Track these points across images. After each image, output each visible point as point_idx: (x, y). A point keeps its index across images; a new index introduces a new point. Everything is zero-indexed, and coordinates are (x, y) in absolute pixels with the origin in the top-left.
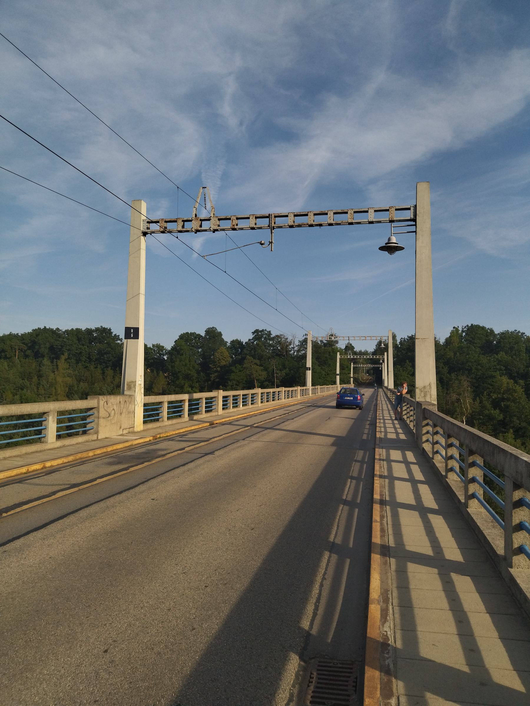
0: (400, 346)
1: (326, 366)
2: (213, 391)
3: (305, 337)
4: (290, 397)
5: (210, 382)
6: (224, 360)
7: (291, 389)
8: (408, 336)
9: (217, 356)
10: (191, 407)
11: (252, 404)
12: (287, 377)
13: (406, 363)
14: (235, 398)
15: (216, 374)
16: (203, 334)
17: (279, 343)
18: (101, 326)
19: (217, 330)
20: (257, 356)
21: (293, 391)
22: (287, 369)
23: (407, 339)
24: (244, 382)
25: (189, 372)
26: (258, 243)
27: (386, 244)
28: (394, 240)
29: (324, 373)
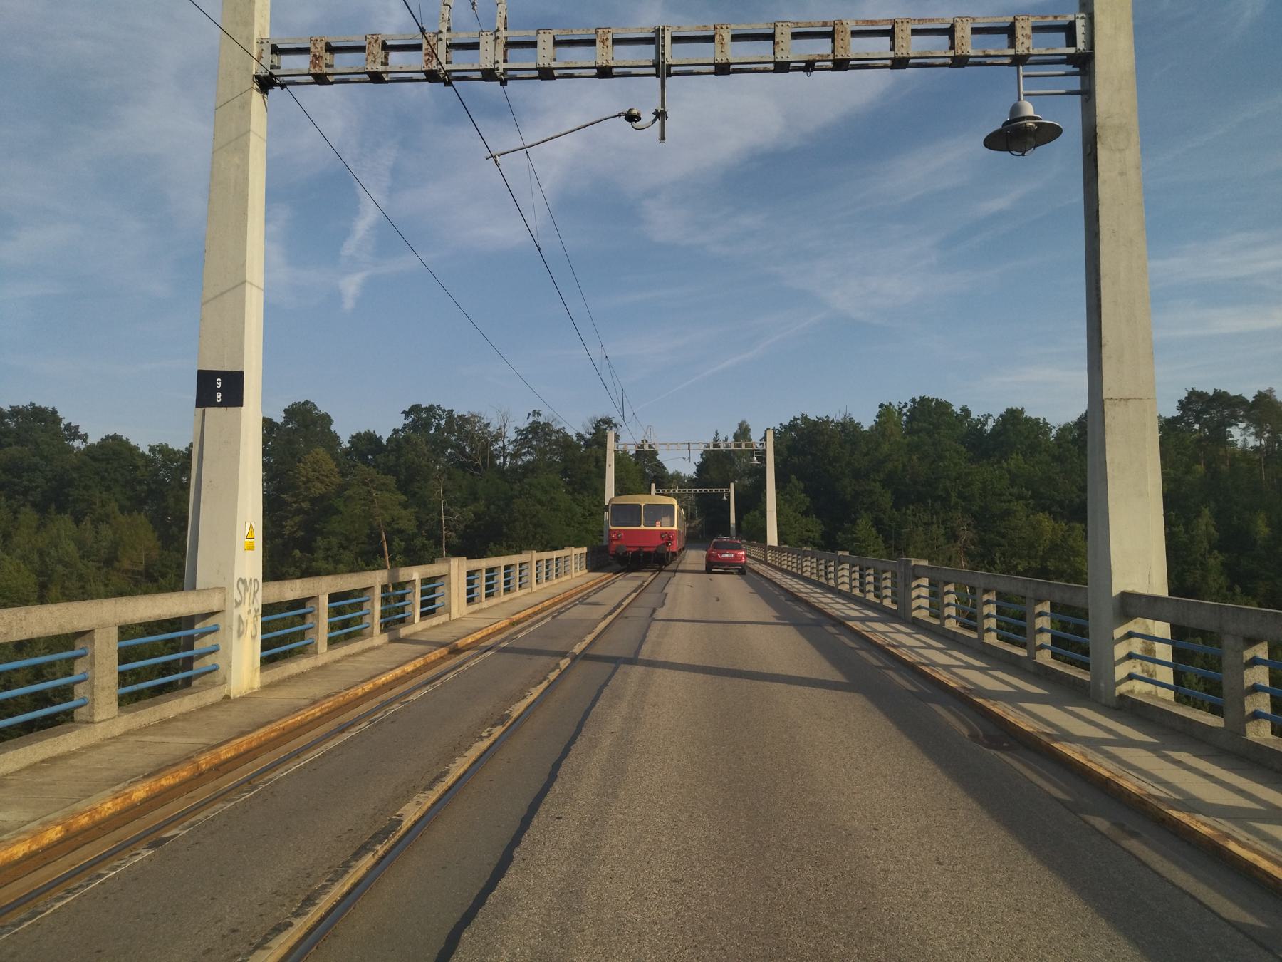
0: (1051, 440)
1: (586, 493)
2: (523, 552)
3: (532, 419)
4: (561, 573)
5: (278, 541)
6: (322, 482)
7: (554, 554)
8: (781, 424)
10: (270, 618)
11: (488, 596)
13: (790, 482)
14: (395, 595)
15: (297, 519)
17: (469, 437)
18: (32, 404)
19: (316, 408)
20: (403, 470)
21: (550, 562)
22: (482, 502)
23: (779, 431)
24: (363, 538)
26: (619, 115)
27: (1006, 124)
28: (1029, 109)
29: (579, 510)
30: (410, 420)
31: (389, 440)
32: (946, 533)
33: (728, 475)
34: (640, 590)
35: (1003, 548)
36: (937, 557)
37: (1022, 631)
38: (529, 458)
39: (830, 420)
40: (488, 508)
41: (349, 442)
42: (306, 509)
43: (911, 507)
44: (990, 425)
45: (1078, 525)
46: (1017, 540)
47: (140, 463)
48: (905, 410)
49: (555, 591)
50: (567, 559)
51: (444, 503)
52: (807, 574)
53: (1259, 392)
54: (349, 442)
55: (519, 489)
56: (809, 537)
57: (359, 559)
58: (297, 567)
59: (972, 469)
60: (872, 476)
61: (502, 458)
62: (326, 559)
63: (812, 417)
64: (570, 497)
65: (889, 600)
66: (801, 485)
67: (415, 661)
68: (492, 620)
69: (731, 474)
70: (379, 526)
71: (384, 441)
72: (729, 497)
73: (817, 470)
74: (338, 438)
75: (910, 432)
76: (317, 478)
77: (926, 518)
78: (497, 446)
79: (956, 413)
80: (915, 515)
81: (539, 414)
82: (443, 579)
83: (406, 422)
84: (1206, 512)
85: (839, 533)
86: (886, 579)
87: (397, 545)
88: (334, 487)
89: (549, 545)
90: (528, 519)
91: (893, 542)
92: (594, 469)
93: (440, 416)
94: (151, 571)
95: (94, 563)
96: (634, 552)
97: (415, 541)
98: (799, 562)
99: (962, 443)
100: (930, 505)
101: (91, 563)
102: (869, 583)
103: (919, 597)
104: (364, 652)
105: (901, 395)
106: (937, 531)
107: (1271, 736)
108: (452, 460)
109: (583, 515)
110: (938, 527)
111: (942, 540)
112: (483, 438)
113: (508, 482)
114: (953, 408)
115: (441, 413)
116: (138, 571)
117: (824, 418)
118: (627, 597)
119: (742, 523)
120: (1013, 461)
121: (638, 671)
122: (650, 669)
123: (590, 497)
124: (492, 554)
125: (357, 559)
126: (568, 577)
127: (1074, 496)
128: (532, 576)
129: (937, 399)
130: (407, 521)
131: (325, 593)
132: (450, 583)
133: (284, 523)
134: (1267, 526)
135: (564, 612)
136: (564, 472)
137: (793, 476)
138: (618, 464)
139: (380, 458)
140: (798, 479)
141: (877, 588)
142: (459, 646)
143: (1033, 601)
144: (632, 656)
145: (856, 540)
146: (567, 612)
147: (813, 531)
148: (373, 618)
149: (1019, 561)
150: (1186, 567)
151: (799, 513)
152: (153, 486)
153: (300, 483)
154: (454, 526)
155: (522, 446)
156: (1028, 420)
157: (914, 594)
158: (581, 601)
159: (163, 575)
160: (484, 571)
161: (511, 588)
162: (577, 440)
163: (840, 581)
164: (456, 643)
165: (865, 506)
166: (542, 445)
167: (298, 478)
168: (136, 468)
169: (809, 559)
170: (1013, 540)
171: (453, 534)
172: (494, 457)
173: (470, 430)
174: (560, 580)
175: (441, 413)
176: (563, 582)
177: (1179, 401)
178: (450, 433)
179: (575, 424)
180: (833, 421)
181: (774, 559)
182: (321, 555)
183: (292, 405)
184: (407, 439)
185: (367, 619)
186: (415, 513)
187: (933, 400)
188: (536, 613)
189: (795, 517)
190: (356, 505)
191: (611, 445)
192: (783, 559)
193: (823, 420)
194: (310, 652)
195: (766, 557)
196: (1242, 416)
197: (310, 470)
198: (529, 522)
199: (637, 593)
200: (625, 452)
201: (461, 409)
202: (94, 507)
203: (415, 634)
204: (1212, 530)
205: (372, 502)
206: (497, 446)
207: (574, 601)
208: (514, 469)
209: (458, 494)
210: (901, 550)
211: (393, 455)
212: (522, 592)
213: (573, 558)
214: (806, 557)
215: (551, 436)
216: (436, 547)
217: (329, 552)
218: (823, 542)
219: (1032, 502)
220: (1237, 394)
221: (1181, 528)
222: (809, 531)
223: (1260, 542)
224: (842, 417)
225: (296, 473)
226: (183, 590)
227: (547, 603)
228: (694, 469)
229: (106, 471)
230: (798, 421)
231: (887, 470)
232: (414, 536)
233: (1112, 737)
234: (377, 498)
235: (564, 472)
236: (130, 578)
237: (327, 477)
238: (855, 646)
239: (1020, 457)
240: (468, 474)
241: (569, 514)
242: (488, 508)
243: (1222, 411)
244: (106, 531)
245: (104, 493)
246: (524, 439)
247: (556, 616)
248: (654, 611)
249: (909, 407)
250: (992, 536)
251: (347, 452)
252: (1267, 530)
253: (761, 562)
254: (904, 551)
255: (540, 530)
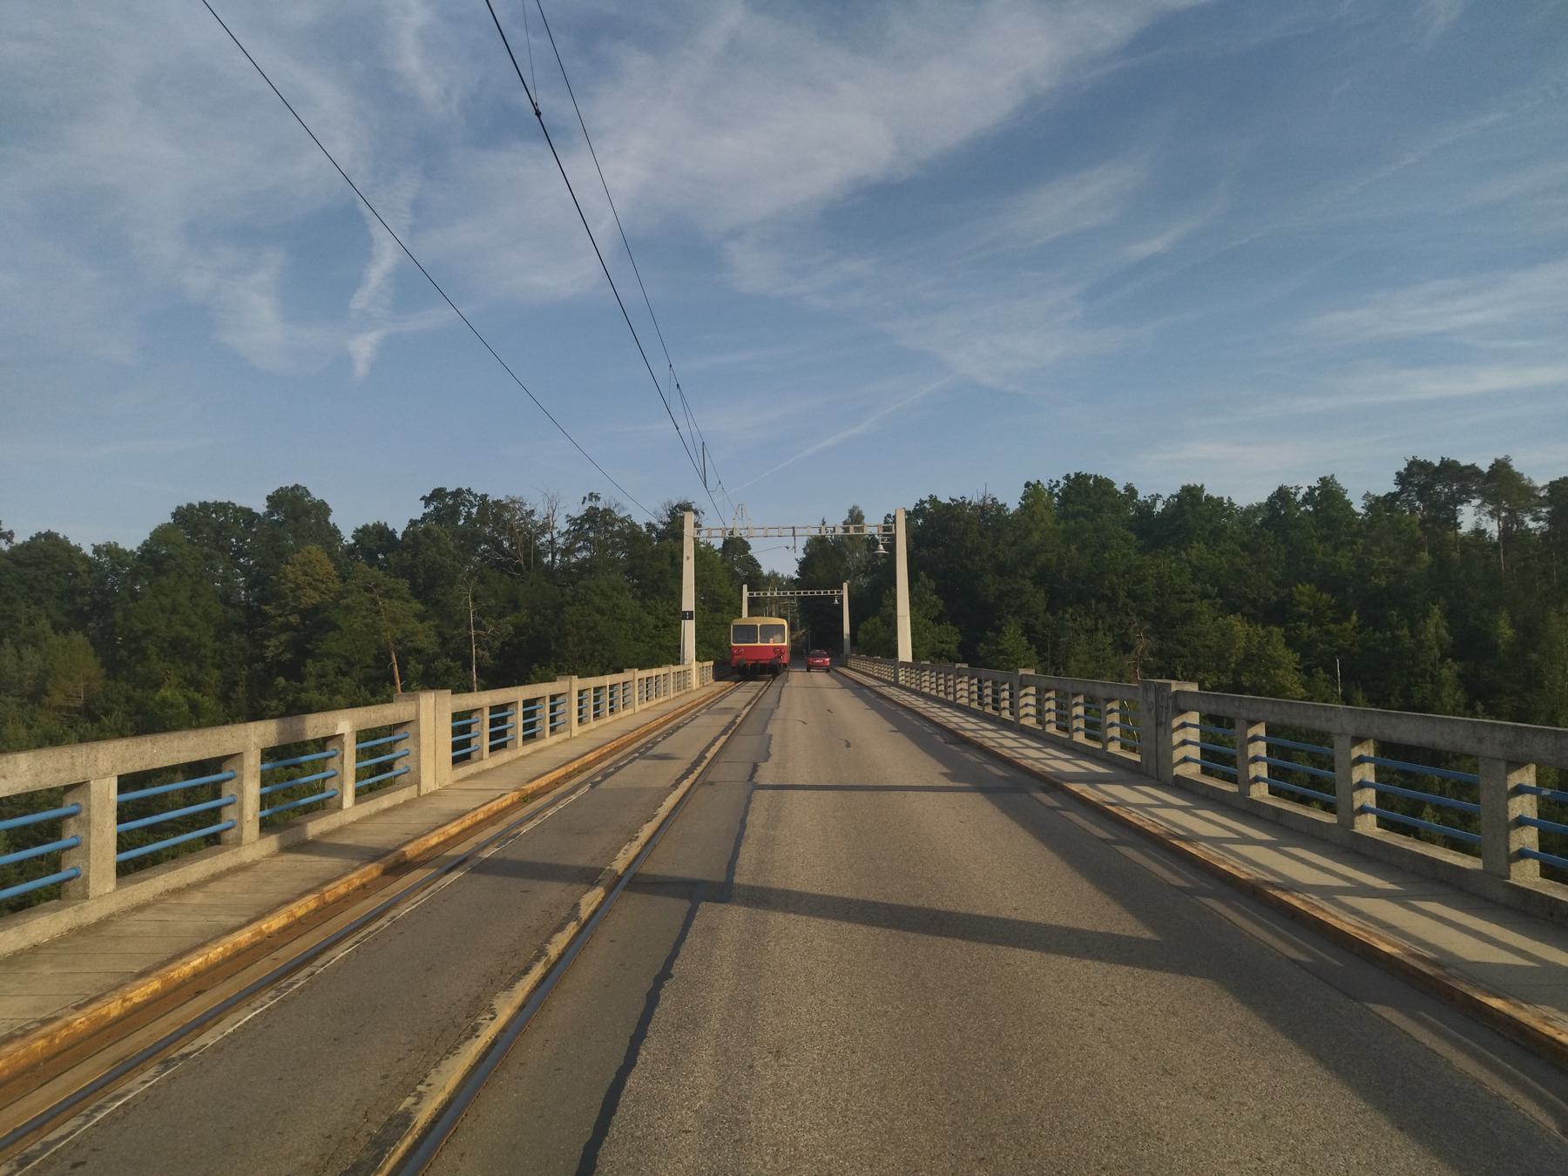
1: (659, 598)
3: (588, 505)
5: (258, 666)
6: (316, 589)
7: (608, 680)
9: (291, 576)
12: (521, 638)
14: (499, 714)
15: (283, 637)
16: (260, 507)
17: (507, 528)
20: (422, 572)
21: (585, 693)
24: (370, 661)
25: (186, 632)
30: (432, 508)
31: (404, 534)
32: (1115, 641)
33: (838, 574)
34: (757, 699)
35: (1185, 660)
36: (1104, 672)
37: (1230, 760)
38: (585, 554)
39: (967, 502)
40: (532, 619)
41: (353, 537)
42: (295, 624)
43: (1070, 610)
44: (1159, 507)
45: (1276, 629)
46: (1201, 650)
47: (81, 568)
48: (1056, 490)
49: (606, 735)
50: (626, 686)
51: (474, 613)
52: (964, 701)
53: (1497, 461)
54: (353, 537)
55: (573, 593)
56: (943, 650)
57: (363, 688)
58: (281, 700)
59: (1143, 561)
60: (1021, 572)
61: (550, 555)
62: (319, 688)
63: (944, 499)
64: (638, 603)
65: (1118, 744)
66: (933, 584)
67: (293, 907)
68: (492, 793)
69: (842, 573)
70: (388, 644)
71: (399, 536)
72: (841, 600)
73: (951, 565)
74: (338, 532)
75: (1065, 516)
76: (310, 584)
77: (1089, 623)
78: (543, 540)
79: (1119, 492)
80: (1075, 620)
81: (598, 498)
82: (406, 729)
83: (426, 511)
84: (1436, 610)
85: (982, 645)
86: (1111, 711)
87: (413, 669)
88: (332, 595)
89: (612, 666)
90: (583, 632)
91: (1047, 654)
92: (669, 568)
93: (470, 502)
94: (92, 707)
95: (14, 699)
96: (752, 665)
97: (436, 663)
98: (918, 677)
99: (1130, 529)
100: (1093, 606)
101: (10, 699)
102: (1077, 717)
103: (1184, 743)
104: (216, 877)
105: (1052, 472)
106: (1105, 640)
107: (1539, 879)
108: (487, 558)
109: (656, 627)
110: (1105, 634)
111: (1109, 651)
112: (526, 529)
113: (559, 586)
114: (1115, 487)
115: (472, 499)
116: (76, 708)
117: (959, 499)
118: (713, 743)
119: (859, 632)
120: (1193, 551)
121: (734, 917)
122: (759, 914)
123: (664, 604)
124: (536, 678)
125: (359, 688)
126: (629, 712)
127: (1271, 593)
128: (571, 713)
129: (1096, 476)
130: (425, 638)
131: (106, 775)
132: (419, 735)
133: (266, 643)
134: (1511, 627)
135: (613, 773)
136: (630, 571)
137: (922, 573)
138: (700, 561)
139: (393, 558)
140: (929, 577)
141: (996, 701)
142: (409, 855)
143: (1502, 766)
144: (722, 878)
145: (1002, 652)
146: (618, 773)
147: (947, 642)
148: (241, 811)
149: (1206, 675)
150: (1412, 679)
151: (929, 619)
152: (98, 598)
153: (287, 591)
154: (487, 643)
155: (576, 539)
156: (1209, 499)
157: (1177, 738)
158: (643, 753)
159: (107, 713)
160: (487, 711)
161: (537, 734)
162: (648, 531)
163: (1022, 712)
164: (404, 849)
165: (1013, 610)
166: (602, 538)
167: (283, 584)
168: (76, 574)
169: (966, 679)
170: (1197, 649)
171: (487, 654)
172: (539, 554)
173: (508, 520)
174: (616, 716)
175: (472, 499)
176: (620, 719)
177: (1397, 474)
178: (484, 524)
179: (644, 512)
180: (970, 503)
181: (908, 679)
182: (313, 684)
183: (278, 491)
184: (426, 532)
185: (332, 785)
186: (436, 626)
187: (1090, 477)
188: (568, 776)
189: (925, 625)
190: (356, 617)
191: (689, 531)
192: (923, 679)
193: (957, 501)
194: (72, 895)
195: (896, 677)
196: (1475, 491)
197: (300, 573)
198: (584, 636)
199: (727, 737)
200: (709, 546)
201: (497, 493)
202: (18, 625)
203: (341, 830)
204: (1443, 632)
205: (378, 612)
206: (543, 540)
207: (633, 752)
208: (566, 569)
209: (492, 602)
210: (1059, 663)
211: (408, 552)
212: (556, 738)
213: (637, 684)
214: (961, 676)
215: (613, 525)
216: (465, 671)
217: (323, 679)
218: (960, 656)
219: (1219, 601)
220: (1469, 464)
221: (1406, 631)
222: (942, 642)
223: (1503, 647)
224: (981, 498)
225: (282, 578)
226: (392, 702)
227: (591, 757)
228: (796, 566)
229: (36, 578)
230: (925, 505)
231: (1039, 564)
232: (435, 657)
233: (1532, 964)
234: (384, 608)
235: (630, 571)
236: (65, 717)
237: (323, 582)
238: (1109, 837)
239: (1202, 545)
240: (506, 576)
241: (637, 625)
242: (532, 619)
243: (1451, 486)
244: (32, 657)
245: (33, 607)
246: (578, 530)
247: (599, 782)
248: (755, 768)
249: (1061, 485)
250: (1171, 644)
251: (350, 550)
252: (1510, 632)
253: (890, 684)
254: (1063, 665)
255: (599, 647)
